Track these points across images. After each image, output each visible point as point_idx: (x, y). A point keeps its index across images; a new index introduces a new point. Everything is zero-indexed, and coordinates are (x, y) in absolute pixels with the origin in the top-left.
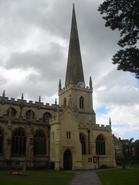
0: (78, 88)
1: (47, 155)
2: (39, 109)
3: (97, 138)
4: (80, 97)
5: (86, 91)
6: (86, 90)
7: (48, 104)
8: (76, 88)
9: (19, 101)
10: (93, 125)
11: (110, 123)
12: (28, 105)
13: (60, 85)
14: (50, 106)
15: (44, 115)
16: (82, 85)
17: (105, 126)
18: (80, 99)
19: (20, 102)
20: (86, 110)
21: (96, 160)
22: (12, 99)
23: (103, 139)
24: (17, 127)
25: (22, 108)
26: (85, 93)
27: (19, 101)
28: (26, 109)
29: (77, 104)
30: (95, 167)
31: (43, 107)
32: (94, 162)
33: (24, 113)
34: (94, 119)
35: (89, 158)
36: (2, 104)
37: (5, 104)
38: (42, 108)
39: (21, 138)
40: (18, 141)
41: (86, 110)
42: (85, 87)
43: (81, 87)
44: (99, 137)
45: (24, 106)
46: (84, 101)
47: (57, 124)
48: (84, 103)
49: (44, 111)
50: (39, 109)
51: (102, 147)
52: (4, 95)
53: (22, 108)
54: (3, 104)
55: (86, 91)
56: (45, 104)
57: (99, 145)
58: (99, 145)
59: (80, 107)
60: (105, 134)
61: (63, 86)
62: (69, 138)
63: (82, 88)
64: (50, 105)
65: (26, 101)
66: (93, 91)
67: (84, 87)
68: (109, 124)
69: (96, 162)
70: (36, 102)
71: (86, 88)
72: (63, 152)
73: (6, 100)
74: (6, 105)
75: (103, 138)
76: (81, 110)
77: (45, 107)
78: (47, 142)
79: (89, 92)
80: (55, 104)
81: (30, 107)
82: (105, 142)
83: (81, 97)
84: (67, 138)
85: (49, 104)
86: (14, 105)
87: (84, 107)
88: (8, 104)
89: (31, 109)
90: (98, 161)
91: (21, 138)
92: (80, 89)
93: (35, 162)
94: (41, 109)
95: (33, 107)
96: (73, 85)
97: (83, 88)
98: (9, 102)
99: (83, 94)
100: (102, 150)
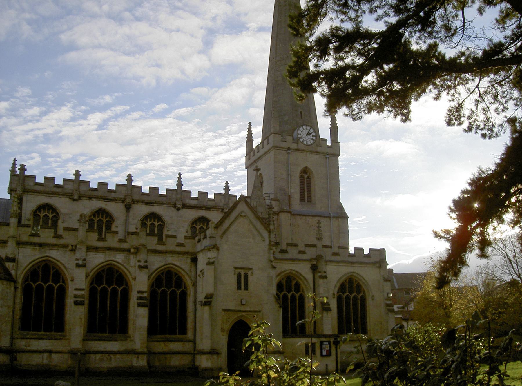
0: (294, 146)
1: (190, 335)
2: (178, 209)
3: (342, 288)
4: (299, 169)
8: (287, 147)
9: (122, 188)
10: (329, 249)
12: (146, 198)
15: (192, 224)
16: (307, 134)
18: (301, 177)
20: (319, 206)
22: (99, 184)
23: (359, 288)
24: (103, 260)
25: (128, 208)
28: (143, 210)
29: (292, 191)
31: (188, 202)
32: (322, 355)
33: (136, 221)
34: (344, 233)
36: (74, 200)
37: (80, 198)
38: (185, 206)
41: (319, 206)
43: (302, 143)
47: (209, 250)
48: (312, 188)
49: (193, 214)
50: (178, 209)
51: (348, 314)
52: (180, 184)
53: (128, 208)
56: (195, 195)
57: (348, 304)
58: (348, 304)
59: (302, 199)
61: (257, 141)
63: (307, 145)
65: (190, 192)
70: (168, 190)
72: (228, 327)
73: (83, 188)
74: (85, 202)
75: (359, 286)
76: (305, 209)
80: (176, 187)
82: (367, 297)
83: (305, 171)
84: (239, 288)
86: (106, 199)
87: (313, 198)
88: (90, 198)
89: (157, 209)
90: (333, 352)
91: (114, 291)
92: (301, 147)
93: (150, 353)
94: (185, 210)
95: (161, 204)
96: (279, 137)
97: (309, 143)
98: (95, 193)
100: (355, 321)
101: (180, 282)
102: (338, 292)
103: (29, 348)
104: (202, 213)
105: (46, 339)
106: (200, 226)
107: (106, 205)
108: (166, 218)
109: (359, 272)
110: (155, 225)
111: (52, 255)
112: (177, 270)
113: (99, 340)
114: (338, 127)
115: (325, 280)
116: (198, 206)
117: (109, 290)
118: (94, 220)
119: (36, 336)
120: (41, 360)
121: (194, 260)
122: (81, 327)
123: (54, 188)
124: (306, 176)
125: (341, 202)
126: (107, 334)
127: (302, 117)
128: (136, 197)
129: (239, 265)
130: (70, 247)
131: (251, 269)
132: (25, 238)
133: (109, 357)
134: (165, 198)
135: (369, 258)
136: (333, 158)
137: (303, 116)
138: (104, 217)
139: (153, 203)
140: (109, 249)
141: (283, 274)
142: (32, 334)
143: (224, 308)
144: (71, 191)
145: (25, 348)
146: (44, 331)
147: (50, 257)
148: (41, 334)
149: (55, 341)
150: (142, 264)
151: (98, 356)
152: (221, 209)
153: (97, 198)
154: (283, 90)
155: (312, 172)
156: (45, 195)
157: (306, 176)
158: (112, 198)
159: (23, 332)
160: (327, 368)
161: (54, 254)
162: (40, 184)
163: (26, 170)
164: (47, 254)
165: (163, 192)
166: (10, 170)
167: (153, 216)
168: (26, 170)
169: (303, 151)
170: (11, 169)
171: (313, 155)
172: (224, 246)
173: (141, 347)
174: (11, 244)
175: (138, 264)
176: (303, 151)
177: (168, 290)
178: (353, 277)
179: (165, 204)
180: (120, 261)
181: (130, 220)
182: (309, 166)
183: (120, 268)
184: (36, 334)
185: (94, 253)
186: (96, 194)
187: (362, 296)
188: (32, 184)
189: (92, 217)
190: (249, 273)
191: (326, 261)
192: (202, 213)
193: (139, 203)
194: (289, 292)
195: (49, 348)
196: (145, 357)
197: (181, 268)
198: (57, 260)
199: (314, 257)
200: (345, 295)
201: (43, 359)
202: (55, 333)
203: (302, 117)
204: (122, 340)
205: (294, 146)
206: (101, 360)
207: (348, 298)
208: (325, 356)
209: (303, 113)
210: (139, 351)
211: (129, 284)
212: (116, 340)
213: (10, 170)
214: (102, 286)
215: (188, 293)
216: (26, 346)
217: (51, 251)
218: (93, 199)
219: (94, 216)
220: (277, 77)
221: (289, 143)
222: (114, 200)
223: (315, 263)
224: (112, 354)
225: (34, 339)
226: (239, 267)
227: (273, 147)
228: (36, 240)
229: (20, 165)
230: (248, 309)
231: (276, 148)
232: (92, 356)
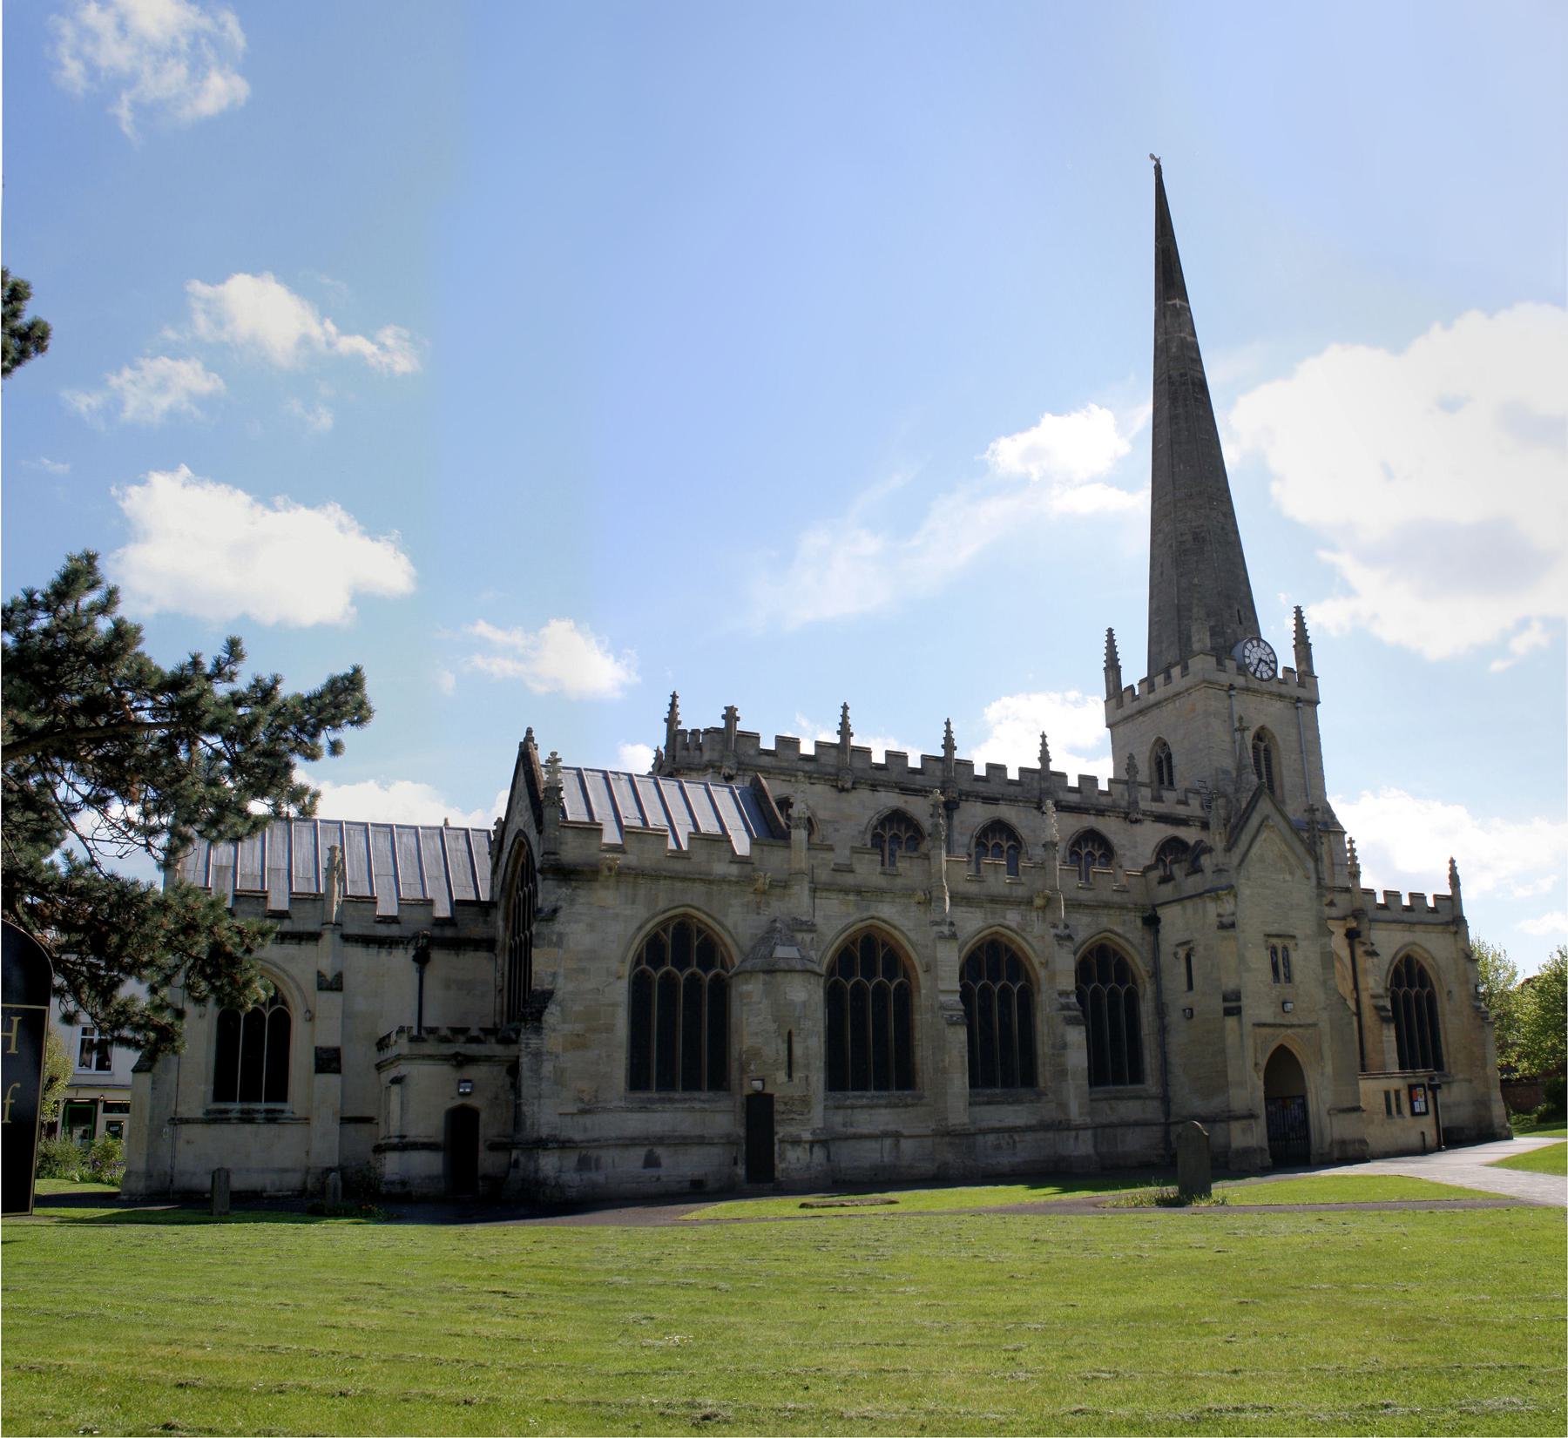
0: (1240, 681)
3: (653, 950)
5: (1281, 696)
6: (1284, 689)
7: (996, 770)
11: (1454, 880)
12: (980, 787)
13: (1113, 666)
14: (1102, 793)
17: (1430, 903)
18: (1254, 747)
19: (938, 773)
21: (1426, 1102)
25: (950, 807)
26: (1278, 706)
27: (932, 765)
28: (975, 815)
30: (1419, 1137)
31: (1063, 796)
32: (1414, 1113)
33: (966, 840)
35: (1387, 1094)
36: (843, 790)
39: (1005, 991)
40: (12, 1008)
42: (1275, 671)
44: (668, 939)
45: (967, 795)
46: (1274, 755)
54: (847, 791)
55: (1281, 696)
56: (1073, 782)
60: (1433, 947)
61: (1134, 671)
62: (1282, 976)
63: (1262, 679)
64: (914, 762)
66: (1322, 697)
67: (1271, 673)
68: (1449, 892)
69: (1426, 1113)
71: (1280, 675)
73: (858, 763)
74: (864, 794)
75: (1422, 971)
77: (1074, 798)
78: (1146, 1008)
79: (1299, 700)
80: (837, 740)
81: (998, 800)
85: (1002, 769)
86: (905, 790)
88: (874, 787)
91: (1005, 991)
92: (1255, 685)
95: (1012, 800)
97: (1265, 676)
98: (881, 775)
99: (1265, 713)
101: (1123, 971)
102: (638, 962)
103: (851, 1130)
104: (1089, 821)
105: (886, 1107)
106: (1087, 850)
107: (906, 802)
108: (1023, 832)
109: (1428, 945)
110: (1002, 846)
111: (881, 915)
112: (1117, 944)
113: (989, 1103)
114: (1310, 645)
115: (1376, 960)
116: (1082, 805)
117: (1016, 991)
118: (882, 836)
119: (865, 1101)
120: (879, 1155)
121: (1152, 922)
122: (964, 1074)
123: (800, 762)
124: (1262, 745)
125: (1328, 799)
126: (998, 1091)
127: (1240, 623)
128: (966, 786)
129: (1274, 929)
130: (920, 896)
131: (1293, 937)
132: (823, 875)
133: (1011, 1141)
134: (1018, 789)
135: (1435, 915)
136: (1308, 709)
137: (1243, 620)
138: (903, 829)
139: (998, 800)
140: (994, 900)
141: (1088, 944)
142: (855, 1097)
143: (1256, 1021)
144: (832, 770)
145: (845, 1129)
146: (875, 1089)
147: (878, 919)
148: (873, 1097)
149: (903, 1110)
150: (1061, 931)
151: (991, 1138)
152: (1125, 813)
153: (888, 786)
154: (1197, 562)
155: (1273, 737)
156: (783, 777)
157: (1262, 745)
158: (918, 787)
159: (833, 1094)
160: (1424, 1140)
161: (887, 911)
162: (767, 753)
163: (738, 719)
164: (872, 913)
165: (1013, 775)
166: (666, 720)
167: (999, 827)
168: (738, 719)
169: (1255, 691)
170: (667, 716)
171: (1273, 702)
172: (1245, 892)
173: (1081, 1114)
174: (801, 892)
175: (1053, 931)
176: (1255, 691)
177: (975, 983)
178: (1411, 953)
179: (1021, 801)
180: (1013, 925)
181: (956, 836)
182: (1269, 726)
183: (1013, 941)
184: (861, 1097)
185: (964, 909)
186: (885, 779)
187: (900, 984)
188: (752, 752)
189: (879, 830)
190: (1290, 944)
191: (1371, 921)
192: (1089, 821)
193: (970, 799)
194: (995, 980)
195: (892, 1127)
196: (1089, 1133)
197: (1127, 940)
198: (895, 927)
199: (1349, 913)
200: (896, 982)
201: (882, 1153)
202: (899, 1093)
203: (1240, 623)
204: (1032, 1101)
205: (1240, 681)
206: (998, 1147)
207: (858, 990)
208: (1420, 1114)
209: (1242, 613)
210: (1078, 1123)
211: (1032, 974)
212: (1018, 1101)
213: (666, 720)
214: (1093, 986)
215: (1141, 993)
216: (844, 1125)
217: (880, 906)
218: (879, 788)
219: (883, 828)
220: (1181, 534)
221: (1230, 676)
222: (920, 791)
223: (1354, 924)
224: (1017, 1132)
225: (862, 1107)
226: (1274, 933)
227: (1204, 681)
228: (849, 879)
229: (726, 708)
230: (1295, 1022)
231: (1210, 683)
232: (980, 1138)
